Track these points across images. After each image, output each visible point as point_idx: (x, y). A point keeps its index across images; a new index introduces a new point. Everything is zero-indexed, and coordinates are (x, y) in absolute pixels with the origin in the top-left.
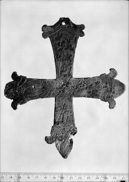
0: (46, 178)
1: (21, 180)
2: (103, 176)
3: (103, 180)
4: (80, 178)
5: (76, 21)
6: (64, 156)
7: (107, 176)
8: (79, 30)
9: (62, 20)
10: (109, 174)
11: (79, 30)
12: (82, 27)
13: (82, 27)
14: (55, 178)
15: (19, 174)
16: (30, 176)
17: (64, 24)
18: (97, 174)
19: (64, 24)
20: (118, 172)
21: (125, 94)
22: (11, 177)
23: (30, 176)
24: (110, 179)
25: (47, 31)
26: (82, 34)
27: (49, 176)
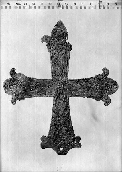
0: (74, 4)
1: (57, 2)
2: (20, 5)
3: (20, 2)
4: (42, 4)
5: (50, 151)
6: (60, 25)
7: (16, 5)
8: (46, 143)
9: (64, 153)
10: (15, 7)
11: (46, 143)
12: (43, 146)
13: (43, 146)
14: (66, 4)
15: (59, 7)
16: (89, 5)
17: (61, 149)
18: (25, 7)
19: (61, 149)
20: (30, 9)
21: (4, 79)
22: (25, 4)
23: (89, 5)
24: (13, 3)
25: (76, 142)
26: (43, 138)
27: (88, 6)
